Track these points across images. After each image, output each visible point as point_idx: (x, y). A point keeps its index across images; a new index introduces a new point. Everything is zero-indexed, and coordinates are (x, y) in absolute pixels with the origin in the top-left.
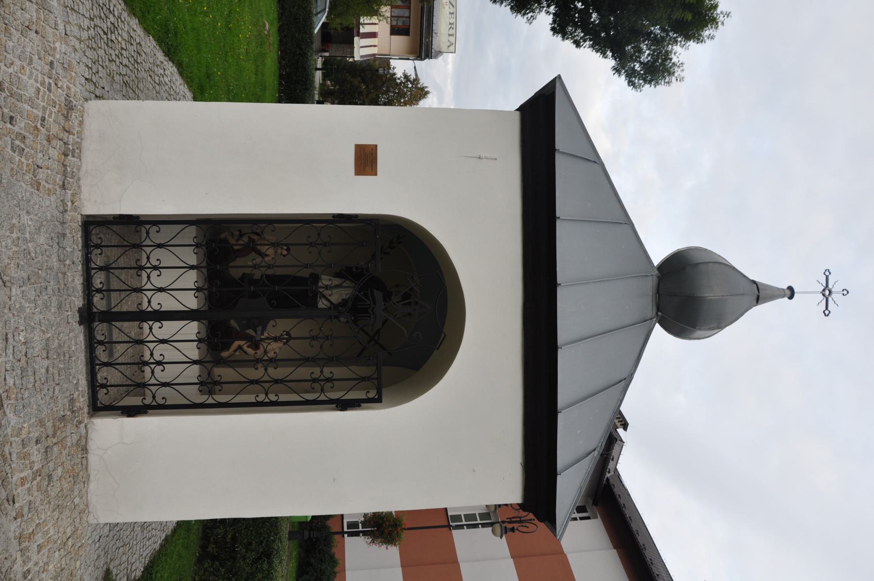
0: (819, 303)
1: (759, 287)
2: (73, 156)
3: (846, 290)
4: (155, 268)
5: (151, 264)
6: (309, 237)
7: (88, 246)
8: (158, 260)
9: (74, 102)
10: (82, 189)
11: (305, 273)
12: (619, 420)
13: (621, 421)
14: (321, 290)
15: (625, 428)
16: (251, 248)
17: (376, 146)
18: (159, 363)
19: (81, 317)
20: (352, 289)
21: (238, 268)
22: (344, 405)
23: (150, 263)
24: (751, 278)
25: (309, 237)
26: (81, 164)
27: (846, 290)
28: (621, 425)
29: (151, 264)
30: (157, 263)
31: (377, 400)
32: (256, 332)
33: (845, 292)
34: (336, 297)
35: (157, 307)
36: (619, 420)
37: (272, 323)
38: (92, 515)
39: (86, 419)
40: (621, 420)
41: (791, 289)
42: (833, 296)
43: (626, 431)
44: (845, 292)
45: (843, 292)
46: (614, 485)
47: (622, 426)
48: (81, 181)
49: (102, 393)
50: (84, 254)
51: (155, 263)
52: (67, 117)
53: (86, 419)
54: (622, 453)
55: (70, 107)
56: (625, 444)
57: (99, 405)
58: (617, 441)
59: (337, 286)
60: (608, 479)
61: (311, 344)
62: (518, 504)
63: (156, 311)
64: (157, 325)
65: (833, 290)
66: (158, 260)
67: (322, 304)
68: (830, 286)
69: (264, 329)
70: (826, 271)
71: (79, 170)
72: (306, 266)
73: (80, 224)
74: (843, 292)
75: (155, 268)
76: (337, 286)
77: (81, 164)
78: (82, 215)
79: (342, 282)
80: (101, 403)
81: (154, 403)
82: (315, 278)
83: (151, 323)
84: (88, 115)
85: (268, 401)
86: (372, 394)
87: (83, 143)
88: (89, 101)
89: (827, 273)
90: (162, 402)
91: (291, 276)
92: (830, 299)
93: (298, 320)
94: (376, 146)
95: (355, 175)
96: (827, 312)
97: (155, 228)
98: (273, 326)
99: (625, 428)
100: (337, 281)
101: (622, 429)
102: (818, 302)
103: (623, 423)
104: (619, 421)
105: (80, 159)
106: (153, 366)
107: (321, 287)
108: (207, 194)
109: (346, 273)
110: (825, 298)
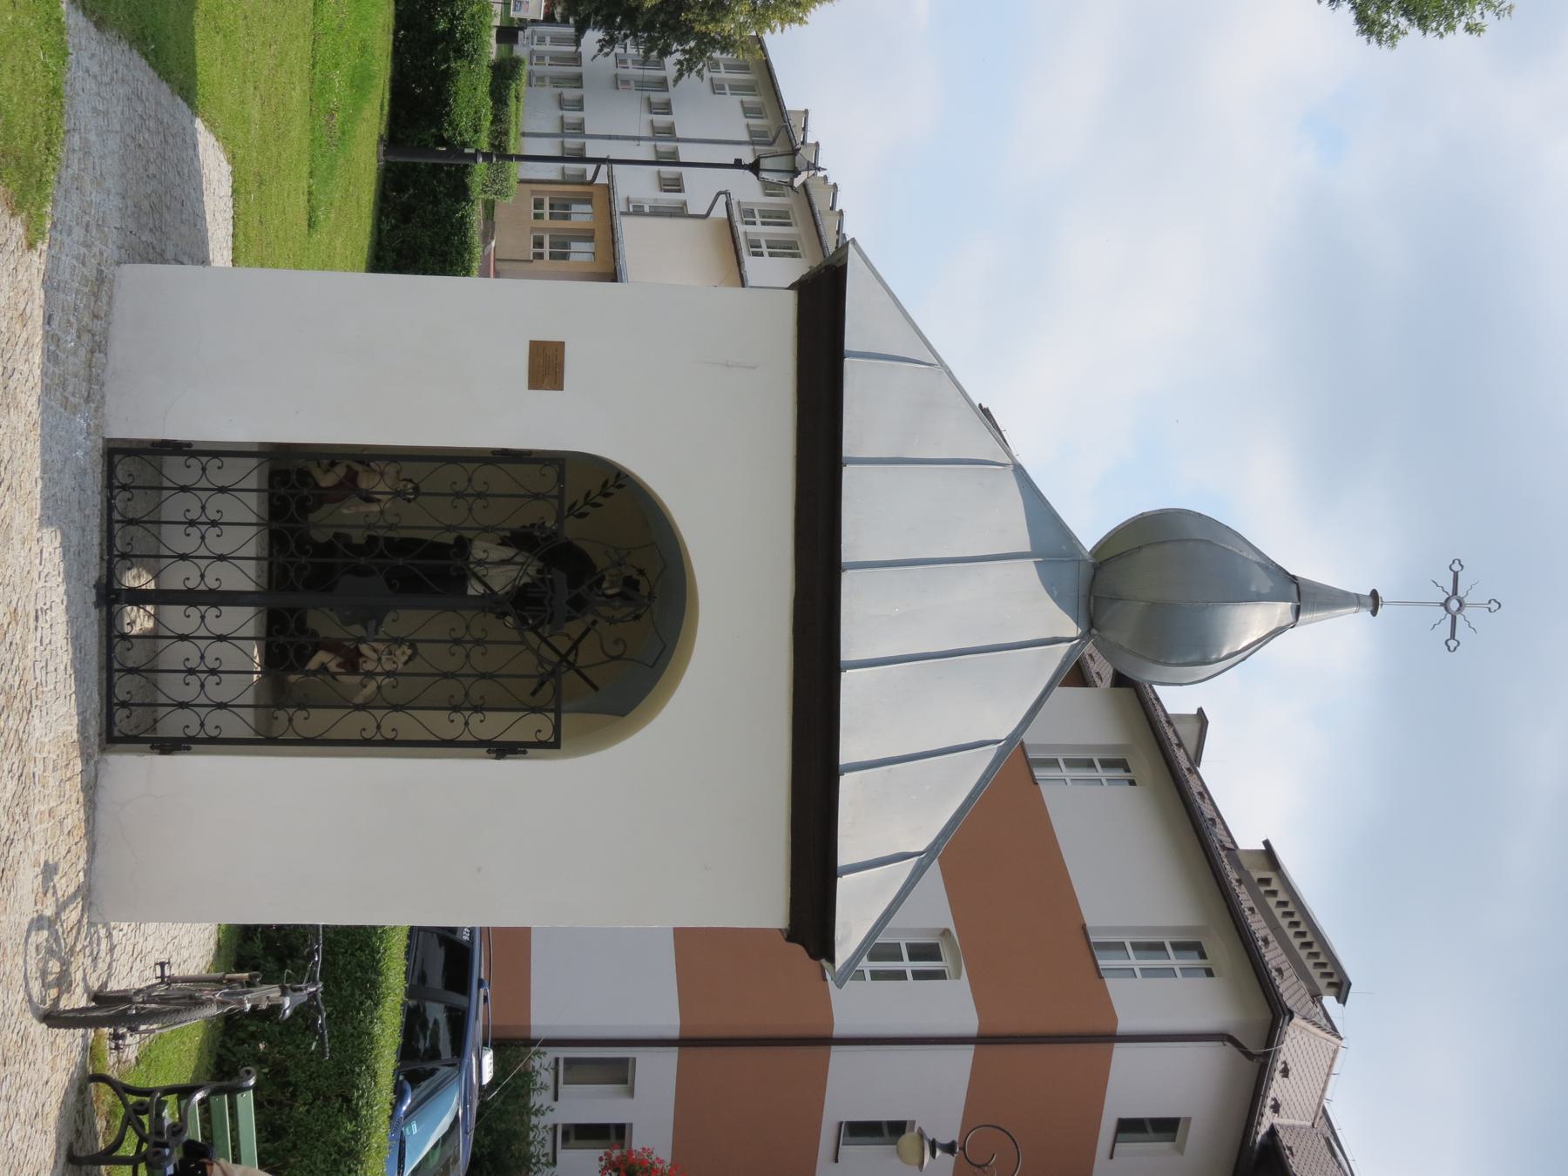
0: (1435, 625)
1: (1301, 588)
2: (100, 352)
3: (1495, 601)
4: (214, 524)
5: (207, 517)
6: (453, 630)
7: (110, 484)
8: (218, 511)
9: (106, 271)
10: (107, 399)
11: (449, 538)
12: (1323, 970)
13: (1330, 975)
14: (472, 566)
15: (1342, 998)
16: (349, 485)
17: (562, 344)
18: (213, 672)
19: (99, 595)
20: (519, 567)
21: (326, 522)
22: (503, 749)
23: (205, 515)
24: (1292, 574)
25: (453, 630)
26: (107, 361)
27: (1495, 601)
28: (1330, 985)
29: (207, 517)
30: (216, 517)
31: (552, 745)
32: (366, 628)
33: (1494, 606)
34: (501, 580)
35: (213, 585)
36: (1323, 970)
37: (391, 616)
38: (95, 907)
39: (96, 755)
40: (1328, 970)
41: (1374, 594)
42: (1466, 611)
43: (1344, 1003)
44: (1494, 606)
45: (1489, 606)
46: (1290, 1149)
47: (1333, 990)
48: (106, 387)
49: (120, 714)
50: (105, 499)
51: (214, 516)
52: (96, 296)
53: (96, 755)
54: (1335, 1070)
55: (101, 279)
56: (1343, 1043)
57: (116, 733)
58: (1291, 1018)
59: (503, 562)
60: (1272, 1132)
61: (454, 504)
62: (780, 930)
63: (212, 591)
64: (213, 611)
65: (1466, 600)
66: (218, 511)
67: (475, 589)
68: (1461, 593)
69: (379, 624)
70: (1454, 562)
71: (103, 371)
72: (449, 528)
73: (101, 452)
74: (1489, 606)
75: (214, 524)
76: (503, 562)
77: (107, 361)
78: (103, 438)
79: (513, 554)
80: (120, 731)
81: (202, 735)
82: (463, 545)
83: (203, 608)
84: (120, 287)
85: (381, 738)
86: (547, 734)
87: (110, 329)
88: (122, 265)
89: (1456, 567)
90: (214, 733)
91: (426, 541)
92: (1459, 617)
93: (431, 613)
94: (562, 344)
95: (529, 388)
96: (1452, 644)
97: (216, 462)
98: (394, 621)
99: (1342, 998)
100: (507, 552)
101: (1333, 998)
102: (1439, 619)
103: (1335, 979)
104: (1324, 975)
105: (106, 354)
106: (203, 676)
107: (472, 563)
108: (297, 412)
109: (520, 540)
110: (1449, 616)
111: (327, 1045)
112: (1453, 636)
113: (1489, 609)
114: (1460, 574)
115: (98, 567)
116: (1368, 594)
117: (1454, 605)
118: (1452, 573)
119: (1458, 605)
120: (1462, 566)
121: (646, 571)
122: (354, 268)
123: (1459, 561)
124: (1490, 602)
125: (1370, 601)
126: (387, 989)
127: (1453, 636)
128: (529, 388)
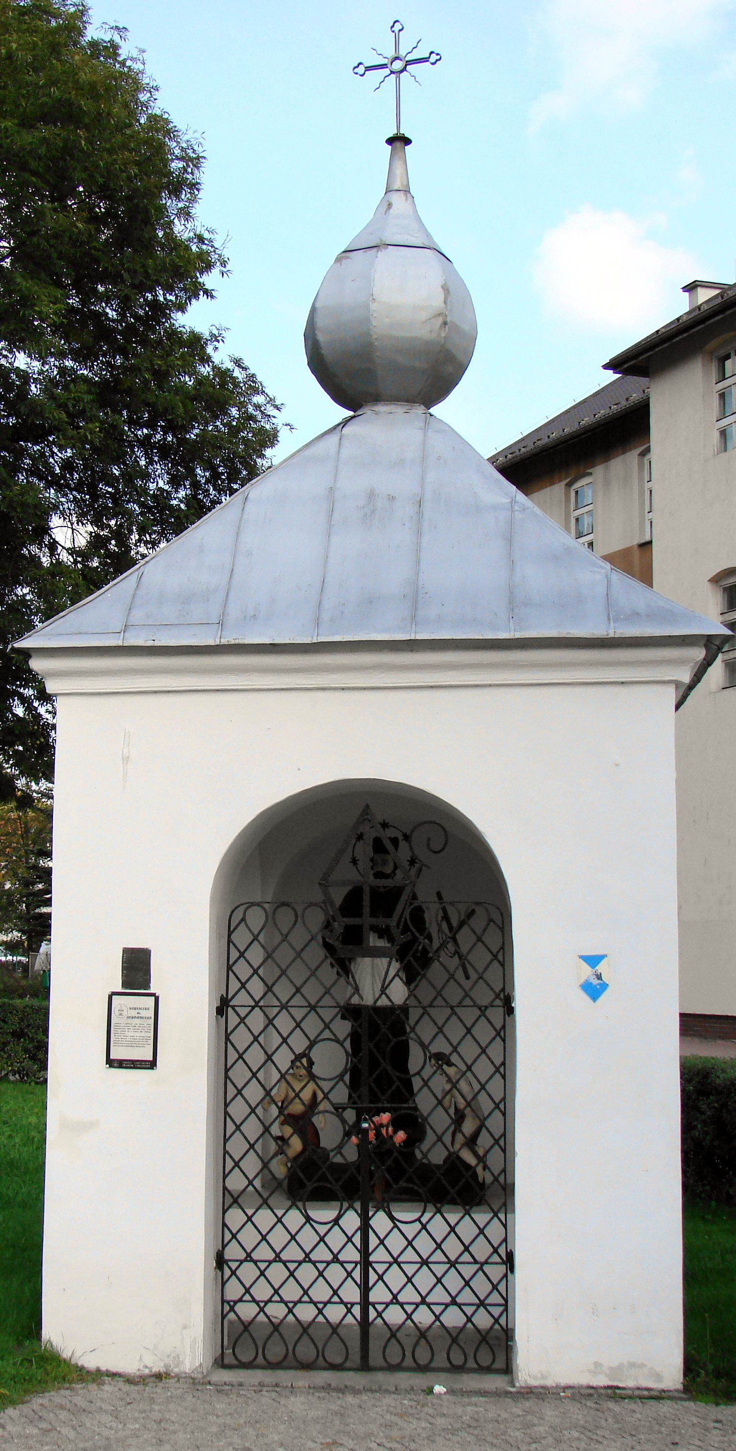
41: (390, 141)
44: (397, 27)
89: (361, 69)
95: (126, 951)
111: (416, 1188)
112: (368, 69)
113: (400, 31)
114: (366, 65)
115: (147, 1371)
116: (390, 147)
117: (398, 65)
118: (367, 72)
119: (397, 61)
120: (360, 64)
121: (386, 821)
122: (683, 996)
123: (440, 59)
124: (393, 31)
125: (398, 144)
126: (282, 1140)
127: (368, 69)
128: (126, 951)
